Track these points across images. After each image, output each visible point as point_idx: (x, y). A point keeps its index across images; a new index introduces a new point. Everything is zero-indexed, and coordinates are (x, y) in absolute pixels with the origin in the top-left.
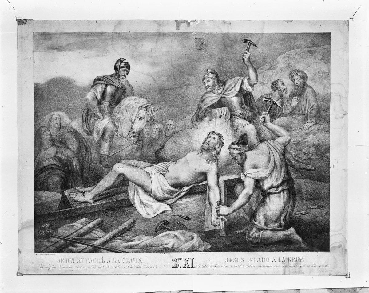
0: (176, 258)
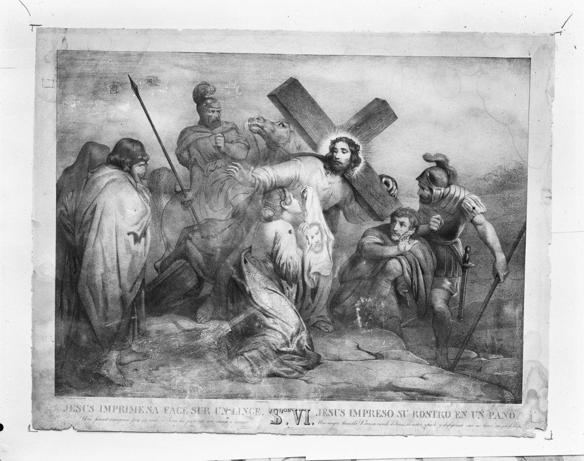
0: (278, 408)
